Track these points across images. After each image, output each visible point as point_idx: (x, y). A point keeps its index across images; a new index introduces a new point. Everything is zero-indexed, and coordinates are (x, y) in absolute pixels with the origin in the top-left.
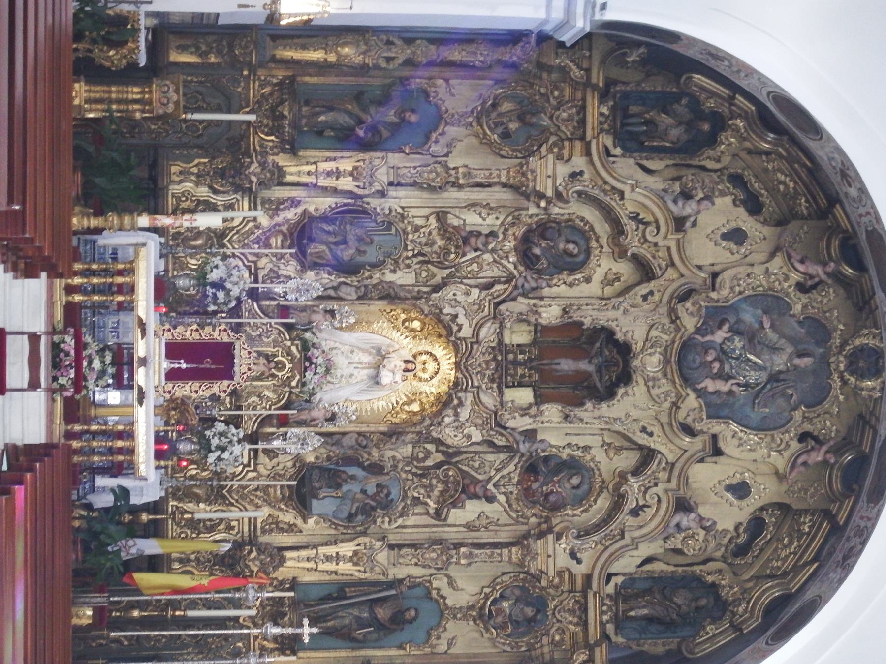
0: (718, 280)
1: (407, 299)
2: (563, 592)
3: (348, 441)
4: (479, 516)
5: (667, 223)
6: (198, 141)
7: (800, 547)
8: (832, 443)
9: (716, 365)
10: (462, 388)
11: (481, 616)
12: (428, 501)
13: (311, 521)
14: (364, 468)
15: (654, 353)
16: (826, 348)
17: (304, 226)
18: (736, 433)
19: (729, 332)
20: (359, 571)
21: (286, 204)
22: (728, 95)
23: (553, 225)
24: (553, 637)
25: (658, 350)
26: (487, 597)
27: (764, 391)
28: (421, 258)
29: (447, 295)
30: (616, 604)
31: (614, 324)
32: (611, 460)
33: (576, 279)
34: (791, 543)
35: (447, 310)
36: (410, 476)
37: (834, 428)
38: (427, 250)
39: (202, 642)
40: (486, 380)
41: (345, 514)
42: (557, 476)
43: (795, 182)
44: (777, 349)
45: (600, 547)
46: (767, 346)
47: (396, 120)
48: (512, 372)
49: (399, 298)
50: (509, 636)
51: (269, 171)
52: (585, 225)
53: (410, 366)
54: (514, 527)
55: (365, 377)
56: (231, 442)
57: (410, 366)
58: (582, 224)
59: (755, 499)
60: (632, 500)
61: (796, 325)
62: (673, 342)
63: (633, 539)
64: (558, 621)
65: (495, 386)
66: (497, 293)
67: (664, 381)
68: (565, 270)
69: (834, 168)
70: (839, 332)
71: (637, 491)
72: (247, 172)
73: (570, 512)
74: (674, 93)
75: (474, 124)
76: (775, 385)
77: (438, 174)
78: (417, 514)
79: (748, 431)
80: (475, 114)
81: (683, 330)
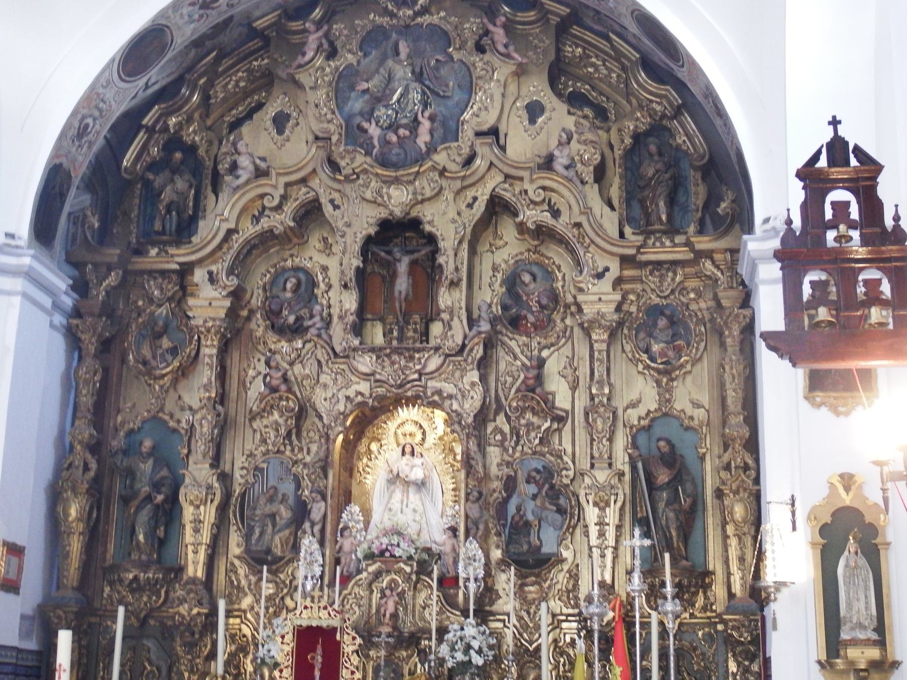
0: (320, 135)
1: (328, 448)
2: (644, 290)
3: (475, 512)
4: (563, 376)
5: (261, 186)
7: (597, 56)
8: (485, 21)
11: (666, 373)
12: (543, 429)
13: (566, 554)
14: (509, 497)
15: (388, 194)
16: (392, 30)
17: (253, 559)
20: (615, 502)
23: (267, 303)
24: (691, 299)
25: (385, 190)
26: (648, 367)
27: (432, 87)
28: (294, 437)
29: (326, 408)
30: (653, 232)
31: (359, 236)
34: (593, 65)
35: (341, 407)
36: (519, 448)
37: (472, 19)
38: (283, 431)
40: (411, 365)
41: (558, 517)
43: (238, 71)
44: (389, 76)
45: (592, 248)
47: (150, 462)
49: (327, 457)
50: (688, 344)
51: (188, 593)
52: (269, 272)
54: (575, 341)
56: (461, 639)
58: (268, 275)
59: (545, 95)
61: (367, 60)
62: (377, 175)
63: (581, 213)
65: (417, 356)
66: (325, 355)
67: (417, 183)
70: (377, 18)
71: (534, 212)
73: (560, 284)
74: (142, 186)
75: (162, 382)
76: (425, 76)
79: (472, 101)
80: (152, 382)
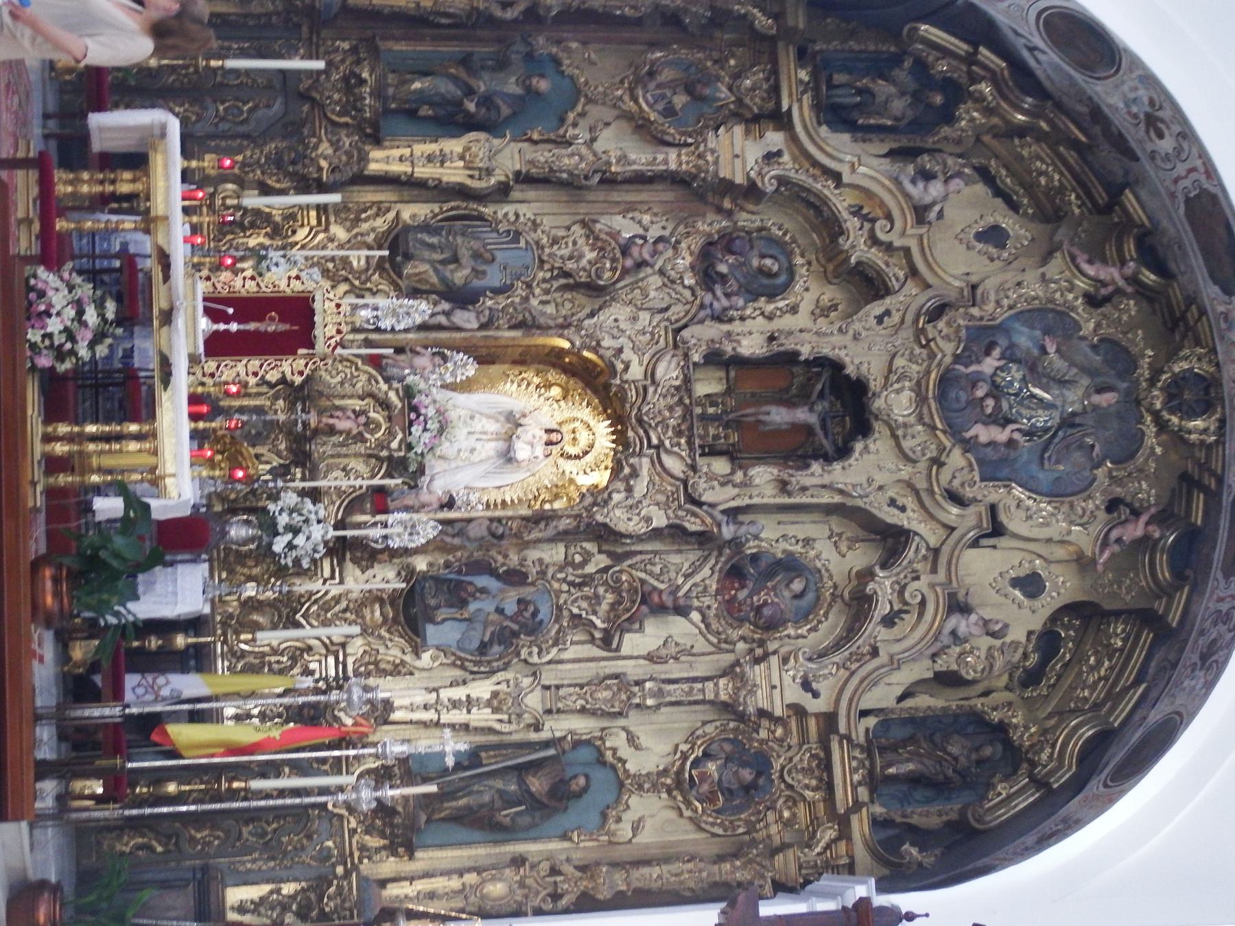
0: (979, 291)
1: (550, 328)
2: (790, 747)
3: (475, 531)
6: (242, 129)
7: (1111, 668)
8: (1153, 510)
9: (990, 403)
10: (634, 451)
11: (679, 783)
12: (593, 618)
13: (426, 656)
14: (498, 577)
15: (902, 389)
17: (397, 237)
18: (1020, 501)
19: (999, 359)
20: (500, 721)
21: (369, 213)
22: (967, 52)
23: (742, 234)
24: (781, 812)
25: (907, 384)
26: (684, 757)
27: (1056, 440)
28: (563, 281)
30: (870, 756)
31: (842, 353)
32: (844, 556)
33: (777, 309)
34: (1099, 663)
36: (565, 587)
38: (570, 265)
39: (274, 843)
40: (670, 433)
41: (475, 644)
42: (770, 579)
43: (1061, 173)
46: (1053, 379)
48: (701, 432)
49: (539, 327)
50: (718, 812)
51: (346, 153)
52: (785, 234)
53: (554, 437)
55: (492, 453)
56: (307, 521)
57: (554, 437)
59: (1052, 598)
60: (883, 602)
61: (1088, 350)
62: (928, 372)
63: (892, 657)
64: (790, 787)
65: (683, 441)
67: (920, 428)
68: (763, 295)
69: (1135, 116)
70: (1147, 360)
71: (889, 591)
72: (313, 155)
73: (791, 631)
75: (626, 98)
76: (1070, 431)
77: (582, 158)
78: (577, 643)
79: (1038, 498)
81: (939, 356)
